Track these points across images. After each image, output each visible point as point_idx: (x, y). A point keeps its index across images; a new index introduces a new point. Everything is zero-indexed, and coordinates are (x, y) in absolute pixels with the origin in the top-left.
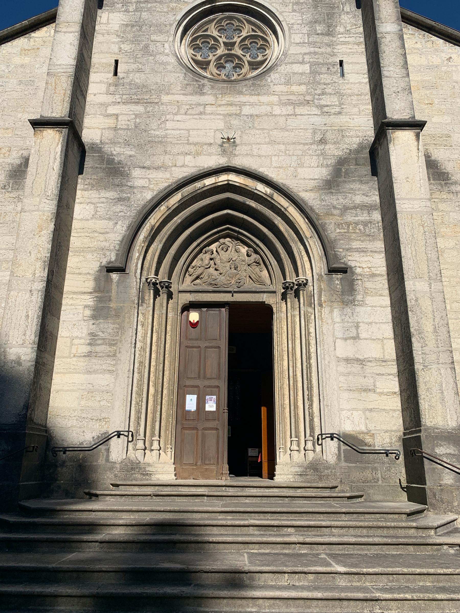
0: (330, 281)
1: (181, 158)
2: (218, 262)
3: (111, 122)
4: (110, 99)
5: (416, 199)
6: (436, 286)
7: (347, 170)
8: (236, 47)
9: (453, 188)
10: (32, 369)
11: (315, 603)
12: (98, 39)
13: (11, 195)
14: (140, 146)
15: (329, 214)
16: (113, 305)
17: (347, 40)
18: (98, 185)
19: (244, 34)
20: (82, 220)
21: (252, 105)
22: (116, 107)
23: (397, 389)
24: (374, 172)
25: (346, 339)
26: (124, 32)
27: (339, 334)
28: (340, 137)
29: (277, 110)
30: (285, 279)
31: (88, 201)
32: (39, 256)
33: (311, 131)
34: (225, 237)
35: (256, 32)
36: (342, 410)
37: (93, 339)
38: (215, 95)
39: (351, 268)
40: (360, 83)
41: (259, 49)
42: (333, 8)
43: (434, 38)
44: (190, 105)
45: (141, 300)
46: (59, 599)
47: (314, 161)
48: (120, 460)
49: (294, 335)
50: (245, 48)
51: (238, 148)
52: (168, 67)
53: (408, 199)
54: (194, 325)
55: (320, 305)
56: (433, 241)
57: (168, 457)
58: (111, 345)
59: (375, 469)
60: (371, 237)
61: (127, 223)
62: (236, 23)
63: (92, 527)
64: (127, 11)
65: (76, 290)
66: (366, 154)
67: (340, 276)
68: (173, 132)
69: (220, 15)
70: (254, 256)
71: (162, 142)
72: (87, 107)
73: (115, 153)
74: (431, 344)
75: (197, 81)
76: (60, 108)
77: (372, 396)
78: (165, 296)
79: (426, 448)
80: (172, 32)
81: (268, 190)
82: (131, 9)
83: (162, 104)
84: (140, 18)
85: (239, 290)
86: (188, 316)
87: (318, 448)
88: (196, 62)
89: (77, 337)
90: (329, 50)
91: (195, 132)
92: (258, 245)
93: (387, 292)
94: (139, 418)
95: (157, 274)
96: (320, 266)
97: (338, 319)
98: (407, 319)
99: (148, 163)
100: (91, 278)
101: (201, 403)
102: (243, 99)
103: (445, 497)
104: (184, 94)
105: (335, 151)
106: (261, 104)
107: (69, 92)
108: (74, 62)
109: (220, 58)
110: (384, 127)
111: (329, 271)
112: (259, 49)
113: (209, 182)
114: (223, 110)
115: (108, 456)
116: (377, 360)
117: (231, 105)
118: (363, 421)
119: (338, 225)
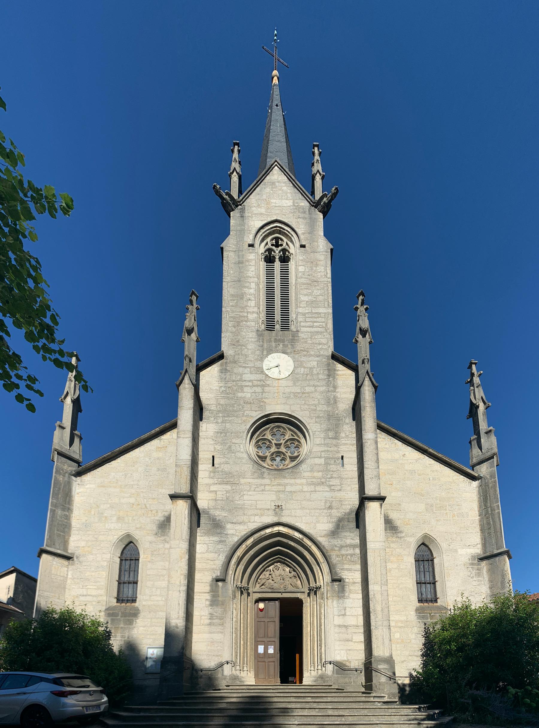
0: (333, 585)
2: (274, 576)
3: (212, 496)
4: (211, 481)
6: (384, 588)
8: (282, 446)
9: (399, 535)
10: (184, 630)
11: (318, 717)
12: (202, 442)
13: (161, 539)
14: (230, 511)
15: (333, 550)
16: (220, 599)
17: (346, 442)
18: (208, 533)
19: (287, 437)
20: (201, 553)
22: (215, 486)
23: (363, 640)
24: (358, 526)
25: (339, 616)
26: (216, 437)
28: (340, 505)
29: (305, 489)
30: (309, 585)
31: (203, 542)
32: (182, 572)
33: (324, 501)
35: (293, 436)
36: (336, 650)
37: (212, 616)
38: (270, 479)
39: (343, 579)
40: (352, 471)
41: (295, 447)
42: (339, 420)
43: (397, 441)
44: (257, 485)
45: (234, 597)
46: (215, 718)
47: (325, 519)
48: (229, 675)
49: (313, 614)
50: (287, 447)
52: (243, 460)
53: (374, 542)
54: (261, 610)
55: (327, 598)
56: (384, 564)
57: (252, 675)
58: (220, 619)
59: (351, 677)
60: (354, 562)
62: (282, 430)
63: (222, 698)
64: (217, 423)
65: (201, 591)
66: (354, 515)
67: (337, 583)
68: (248, 502)
69: (272, 425)
70: (293, 573)
71: (242, 508)
72: (199, 486)
73: (216, 514)
74: (380, 616)
75: (260, 470)
76: (185, 487)
77: (350, 643)
78: (246, 595)
79: (374, 666)
81: (301, 536)
82: (219, 421)
83: (241, 484)
84: (225, 427)
86: (258, 606)
87: (324, 669)
88: (259, 456)
89: (203, 615)
90: (336, 449)
91: (260, 502)
92: (295, 567)
93: (361, 591)
94: (236, 655)
95: (241, 583)
96: (328, 578)
97: (335, 606)
98: (369, 604)
99: (234, 521)
100: (208, 585)
101: (266, 649)
103: (381, 687)
104: (253, 478)
105: (337, 514)
106: (297, 484)
107: (189, 477)
108: (190, 458)
109: (272, 454)
110: (364, 499)
111: (332, 581)
112: (295, 447)
113: (268, 531)
114: (275, 488)
115: (223, 673)
116: (354, 626)
117: (279, 485)
118: (346, 655)
119: (338, 556)
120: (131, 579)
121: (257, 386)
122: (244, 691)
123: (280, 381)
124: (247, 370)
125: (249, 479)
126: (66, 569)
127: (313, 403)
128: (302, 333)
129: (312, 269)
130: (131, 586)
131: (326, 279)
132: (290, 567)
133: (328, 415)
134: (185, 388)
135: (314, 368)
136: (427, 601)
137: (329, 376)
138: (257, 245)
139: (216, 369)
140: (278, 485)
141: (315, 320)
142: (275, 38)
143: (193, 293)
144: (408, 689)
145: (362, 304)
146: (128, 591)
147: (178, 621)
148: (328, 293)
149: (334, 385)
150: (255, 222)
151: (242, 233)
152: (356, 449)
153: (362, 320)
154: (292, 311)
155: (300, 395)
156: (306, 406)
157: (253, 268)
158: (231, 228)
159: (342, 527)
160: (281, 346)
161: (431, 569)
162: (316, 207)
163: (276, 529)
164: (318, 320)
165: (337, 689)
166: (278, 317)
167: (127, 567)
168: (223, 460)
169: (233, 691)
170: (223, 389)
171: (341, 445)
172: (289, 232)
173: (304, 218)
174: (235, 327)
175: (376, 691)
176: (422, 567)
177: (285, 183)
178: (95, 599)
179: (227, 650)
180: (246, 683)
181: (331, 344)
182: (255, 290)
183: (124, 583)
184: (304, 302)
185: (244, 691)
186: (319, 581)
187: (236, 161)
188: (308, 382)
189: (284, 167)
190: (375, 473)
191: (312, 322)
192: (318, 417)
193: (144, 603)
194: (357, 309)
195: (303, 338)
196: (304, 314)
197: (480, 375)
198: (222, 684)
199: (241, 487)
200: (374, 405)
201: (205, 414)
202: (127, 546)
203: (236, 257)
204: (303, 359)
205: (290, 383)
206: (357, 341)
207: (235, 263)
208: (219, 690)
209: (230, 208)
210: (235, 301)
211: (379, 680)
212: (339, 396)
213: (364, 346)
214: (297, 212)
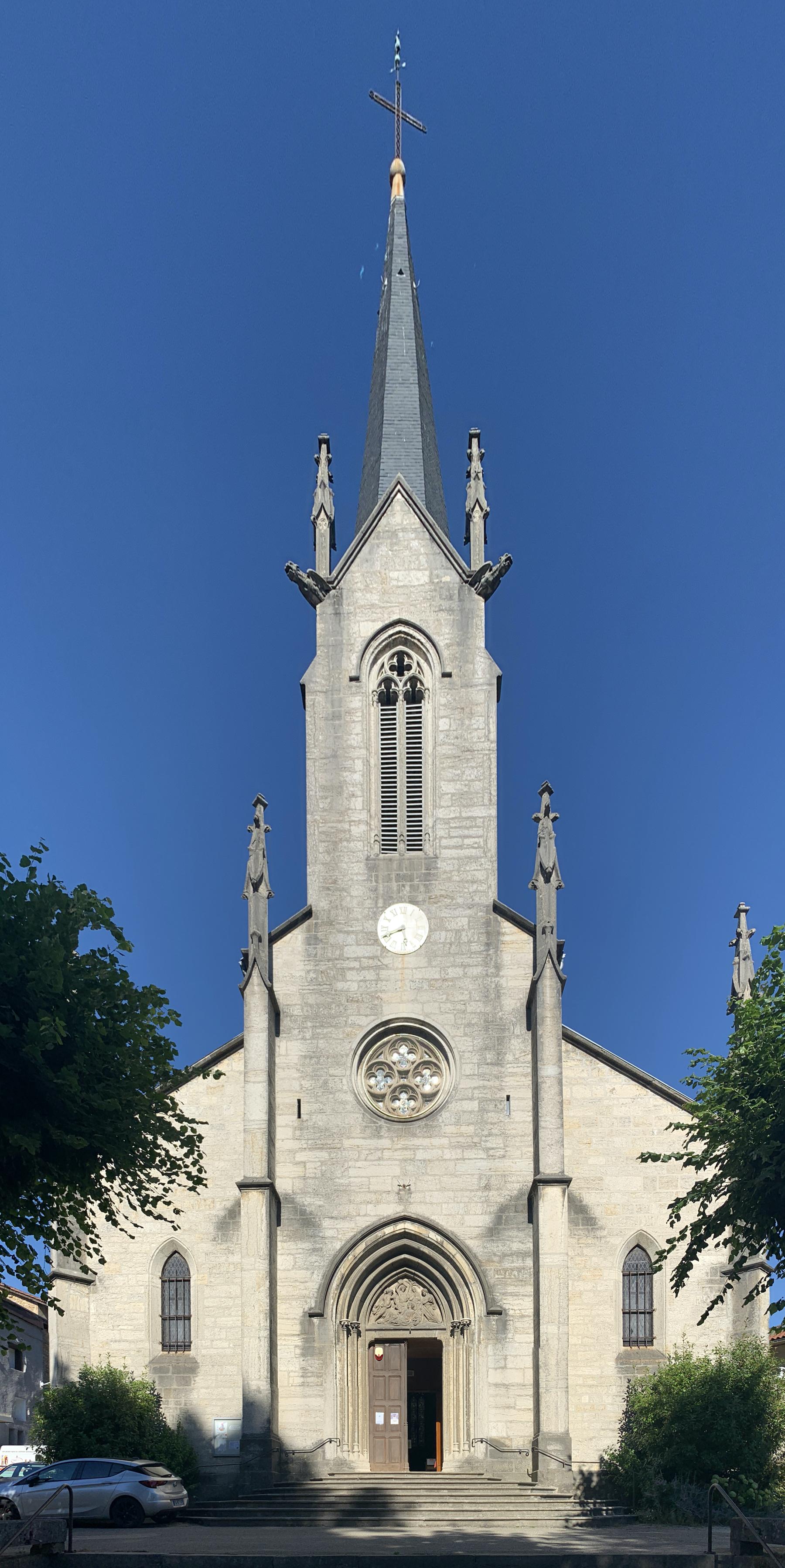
1: (363, 1206)
2: (397, 1302)
3: (299, 1171)
4: (295, 1145)
5: (556, 1254)
6: (563, 1329)
7: (507, 1217)
9: (599, 1233)
13: (222, 1247)
14: (327, 1196)
15: (490, 1261)
17: (515, 1070)
18: (295, 1237)
20: (284, 1270)
21: (425, 1148)
22: (303, 1153)
26: (303, 1065)
27: (491, 1365)
28: (503, 1183)
31: (288, 1252)
33: (476, 1176)
34: (402, 1278)
38: (391, 1138)
39: (505, 1310)
40: (524, 1122)
42: (504, 1030)
45: (338, 1339)
47: (478, 1208)
51: (413, 1195)
53: (550, 1254)
54: (379, 1358)
55: (479, 1342)
57: (365, 1457)
58: (318, 1377)
59: (512, 1462)
61: (322, 1272)
64: (304, 1039)
67: (496, 1317)
70: (429, 1296)
72: (277, 1154)
73: (306, 1203)
74: (553, 1374)
75: (375, 1122)
76: (259, 1167)
77: (512, 1411)
79: (541, 1447)
80: (349, 1065)
82: (308, 1035)
85: (417, 1327)
87: (472, 1449)
90: (497, 1083)
94: (343, 1430)
97: (491, 1353)
100: (298, 1322)
101: (387, 1419)
102: (417, 1142)
103: (549, 1477)
104: (363, 1138)
105: (498, 1198)
106: (433, 1147)
111: (488, 1313)
113: (388, 1230)
114: (399, 1155)
115: (324, 1456)
116: (518, 1385)
117: (406, 1149)
119: (497, 1271)
120: (180, 1313)
121: (369, 968)
122: (356, 1481)
123: (406, 959)
124: (351, 939)
125: (357, 1141)
126: (87, 1299)
127: (460, 998)
128: (444, 860)
129: (462, 722)
130: (181, 1323)
131: (486, 745)
132: (424, 1287)
133: (486, 1021)
134: (253, 993)
135: (464, 930)
136: (637, 1342)
137: (488, 944)
138: (363, 678)
139: (300, 937)
140: (403, 1149)
141: (466, 832)
142: (397, 57)
143: (259, 801)
144: (595, 1479)
145: (547, 814)
146: (177, 1331)
147: (259, 1384)
148: (490, 775)
149: (496, 963)
150: (362, 624)
151: (338, 648)
152: (530, 1082)
153: (545, 847)
154: (427, 813)
155: (438, 984)
156: (449, 1005)
157: (358, 728)
158: (319, 641)
159: (506, 1220)
160: (408, 888)
161: (648, 1289)
162: (472, 584)
163: (401, 1227)
164: (472, 832)
165: (489, 1479)
166: (402, 827)
167: (173, 1292)
168: (316, 1106)
169: (339, 1481)
170: (312, 975)
171: (506, 1076)
172: (422, 643)
173: (450, 610)
174: (329, 853)
175: (542, 1482)
176: (634, 1285)
177: (415, 530)
178: (133, 1346)
179: (332, 1424)
180: (357, 1471)
181: (493, 881)
182: (363, 776)
183: (170, 1319)
184: (446, 797)
185: (356, 1481)
186: (468, 1313)
187: (325, 486)
188: (452, 959)
189: (414, 497)
190: (557, 1136)
191: (460, 837)
192: (469, 1025)
193: (204, 1352)
194: (537, 820)
195: (445, 872)
196: (447, 821)
197: (752, 934)
198: (323, 1471)
199: (345, 1153)
200: (558, 1013)
201: (285, 1023)
202: (169, 1258)
203: (329, 706)
204: (444, 913)
205: (423, 962)
206: (535, 887)
207: (326, 719)
208: (321, 1480)
209: (314, 597)
210: (329, 800)
211: (549, 1466)
212: (504, 985)
213: (547, 896)
214: (437, 599)
